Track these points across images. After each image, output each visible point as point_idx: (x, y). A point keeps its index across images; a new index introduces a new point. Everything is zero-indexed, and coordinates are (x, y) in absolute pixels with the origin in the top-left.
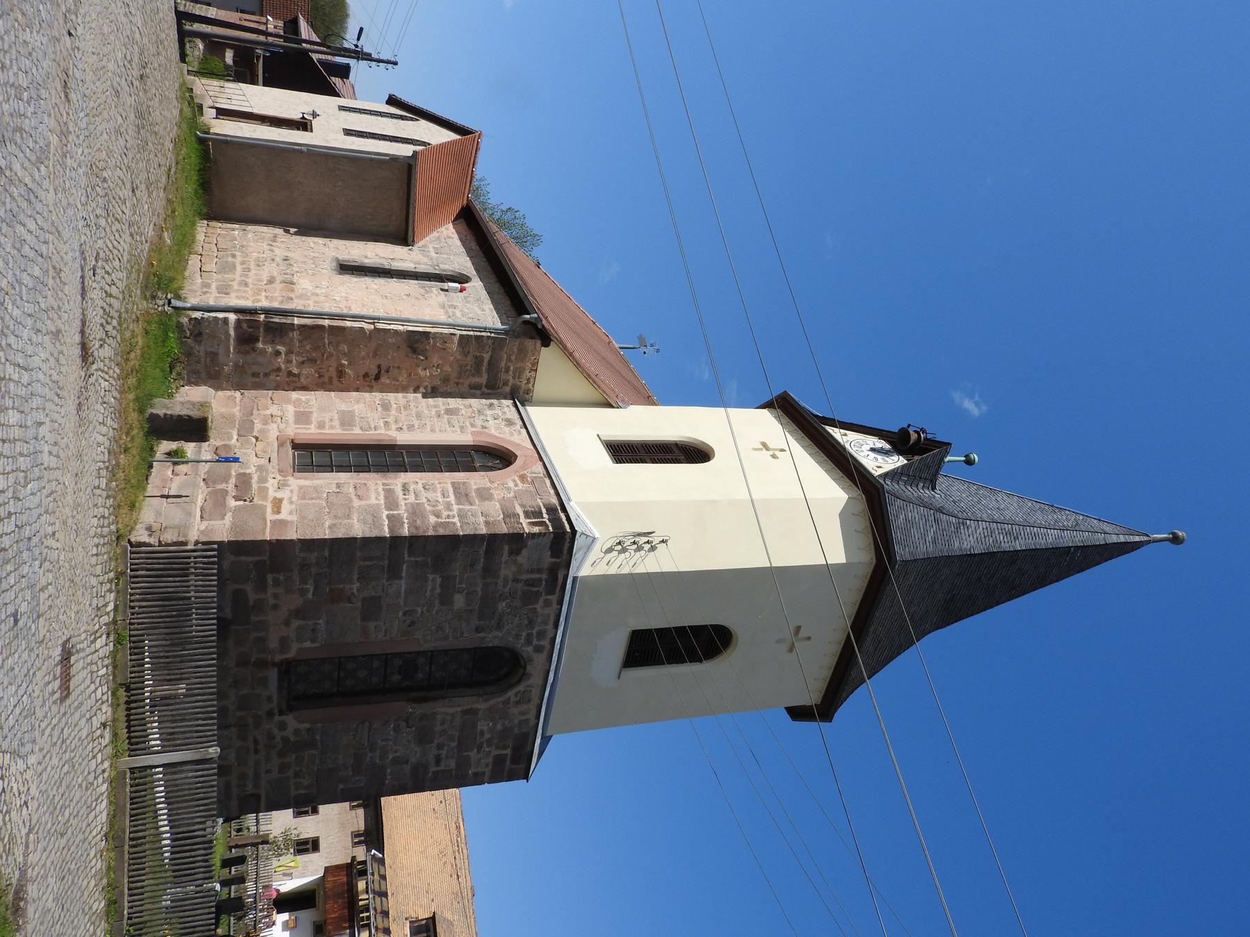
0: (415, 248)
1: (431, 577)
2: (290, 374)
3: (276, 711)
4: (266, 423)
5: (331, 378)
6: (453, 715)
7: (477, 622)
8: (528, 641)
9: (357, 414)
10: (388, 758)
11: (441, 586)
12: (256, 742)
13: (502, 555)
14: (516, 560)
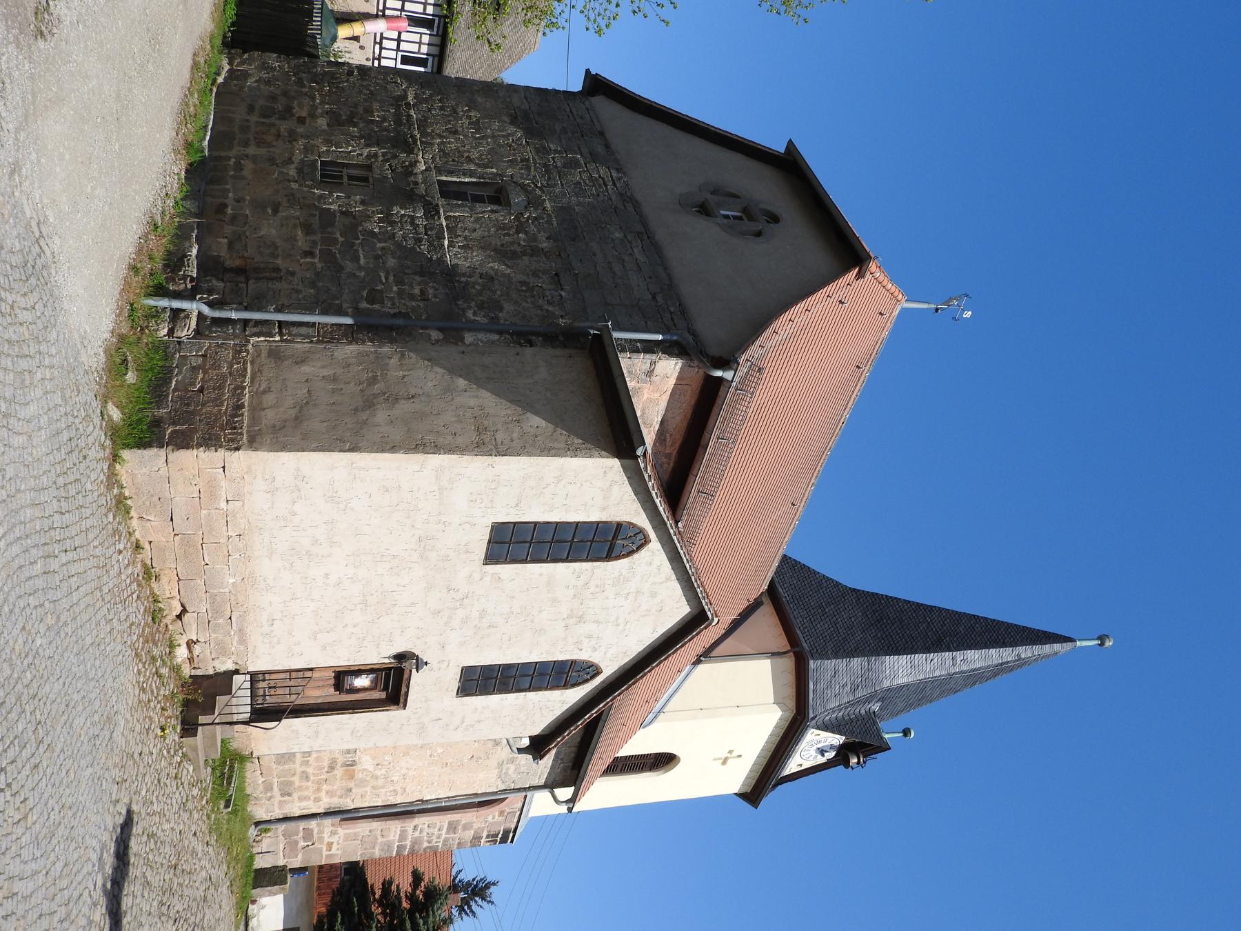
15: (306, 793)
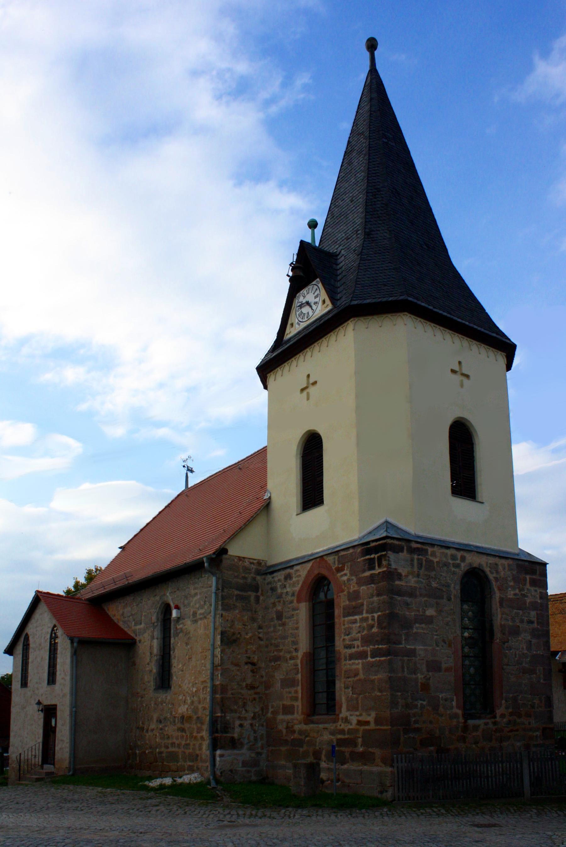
0: (138, 639)
1: (415, 630)
2: (254, 718)
3: (493, 720)
4: (294, 732)
5: (256, 693)
6: (502, 614)
7: (445, 600)
8: (458, 566)
9: (284, 677)
10: (526, 653)
11: (421, 624)
12: (511, 731)
13: (402, 585)
14: (405, 576)
15: (197, 746)
